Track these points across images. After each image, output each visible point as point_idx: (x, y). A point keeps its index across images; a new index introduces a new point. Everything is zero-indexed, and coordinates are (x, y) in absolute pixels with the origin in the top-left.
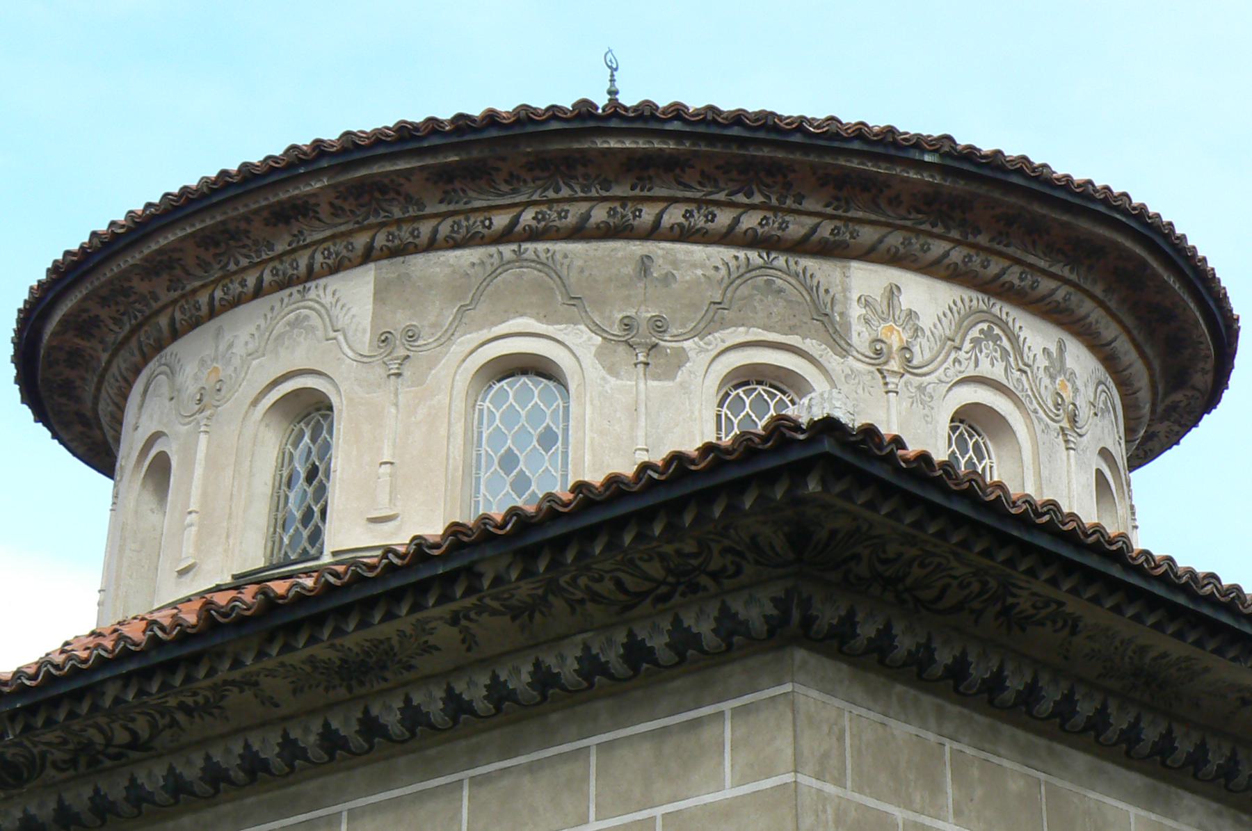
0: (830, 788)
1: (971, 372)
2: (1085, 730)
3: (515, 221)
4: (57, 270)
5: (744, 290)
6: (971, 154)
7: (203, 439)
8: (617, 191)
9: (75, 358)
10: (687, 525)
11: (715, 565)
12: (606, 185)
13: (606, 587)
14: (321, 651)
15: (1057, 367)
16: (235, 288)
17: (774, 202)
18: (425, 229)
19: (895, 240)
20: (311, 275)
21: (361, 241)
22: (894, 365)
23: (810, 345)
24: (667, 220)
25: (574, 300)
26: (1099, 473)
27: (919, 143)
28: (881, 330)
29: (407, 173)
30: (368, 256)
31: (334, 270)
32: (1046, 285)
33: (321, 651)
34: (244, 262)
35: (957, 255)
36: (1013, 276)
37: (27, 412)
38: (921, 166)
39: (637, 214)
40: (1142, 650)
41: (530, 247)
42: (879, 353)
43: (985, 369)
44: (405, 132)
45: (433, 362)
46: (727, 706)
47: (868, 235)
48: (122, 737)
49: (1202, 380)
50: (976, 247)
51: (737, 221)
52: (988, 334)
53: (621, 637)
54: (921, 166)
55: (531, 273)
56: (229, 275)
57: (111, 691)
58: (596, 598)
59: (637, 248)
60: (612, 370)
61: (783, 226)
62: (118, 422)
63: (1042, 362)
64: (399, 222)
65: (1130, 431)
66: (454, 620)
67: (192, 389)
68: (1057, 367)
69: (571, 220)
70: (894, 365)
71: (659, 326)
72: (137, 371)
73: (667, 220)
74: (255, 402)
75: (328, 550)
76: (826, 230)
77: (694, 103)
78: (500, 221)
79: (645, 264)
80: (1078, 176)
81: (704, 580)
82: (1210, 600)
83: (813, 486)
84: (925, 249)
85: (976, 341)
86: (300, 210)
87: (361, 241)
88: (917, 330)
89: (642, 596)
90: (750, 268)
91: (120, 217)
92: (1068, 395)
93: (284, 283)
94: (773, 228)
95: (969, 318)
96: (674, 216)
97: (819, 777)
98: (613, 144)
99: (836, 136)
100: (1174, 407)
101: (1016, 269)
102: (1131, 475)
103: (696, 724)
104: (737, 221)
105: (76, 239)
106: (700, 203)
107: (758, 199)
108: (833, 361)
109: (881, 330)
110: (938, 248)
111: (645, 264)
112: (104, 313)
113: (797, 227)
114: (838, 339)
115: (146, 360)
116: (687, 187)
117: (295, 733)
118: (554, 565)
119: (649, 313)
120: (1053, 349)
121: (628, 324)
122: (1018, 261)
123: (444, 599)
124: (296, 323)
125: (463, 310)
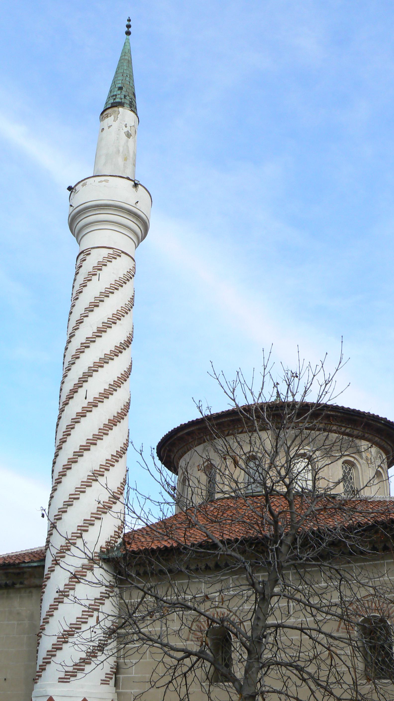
17: (353, 427)
23: (357, 457)
24: (333, 429)
27: (382, 419)
34: (239, 426)
42: (367, 459)
50: (381, 439)
51: (345, 430)
61: (353, 432)
70: (369, 462)
77: (346, 406)
94: (351, 433)
104: (345, 430)
106: (339, 426)
107: (350, 426)
113: (356, 432)
116: (338, 422)
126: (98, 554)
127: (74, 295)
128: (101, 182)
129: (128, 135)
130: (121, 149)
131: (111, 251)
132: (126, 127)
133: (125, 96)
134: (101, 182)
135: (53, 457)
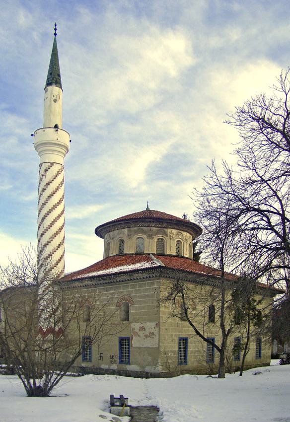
10: (6, 365)
47: (169, 227)
71: (152, 235)
79: (150, 230)
96: (153, 225)
102: (272, 360)
111: (150, 230)
114: (167, 236)
131: (49, 164)
132: (54, 96)
133: (53, 78)
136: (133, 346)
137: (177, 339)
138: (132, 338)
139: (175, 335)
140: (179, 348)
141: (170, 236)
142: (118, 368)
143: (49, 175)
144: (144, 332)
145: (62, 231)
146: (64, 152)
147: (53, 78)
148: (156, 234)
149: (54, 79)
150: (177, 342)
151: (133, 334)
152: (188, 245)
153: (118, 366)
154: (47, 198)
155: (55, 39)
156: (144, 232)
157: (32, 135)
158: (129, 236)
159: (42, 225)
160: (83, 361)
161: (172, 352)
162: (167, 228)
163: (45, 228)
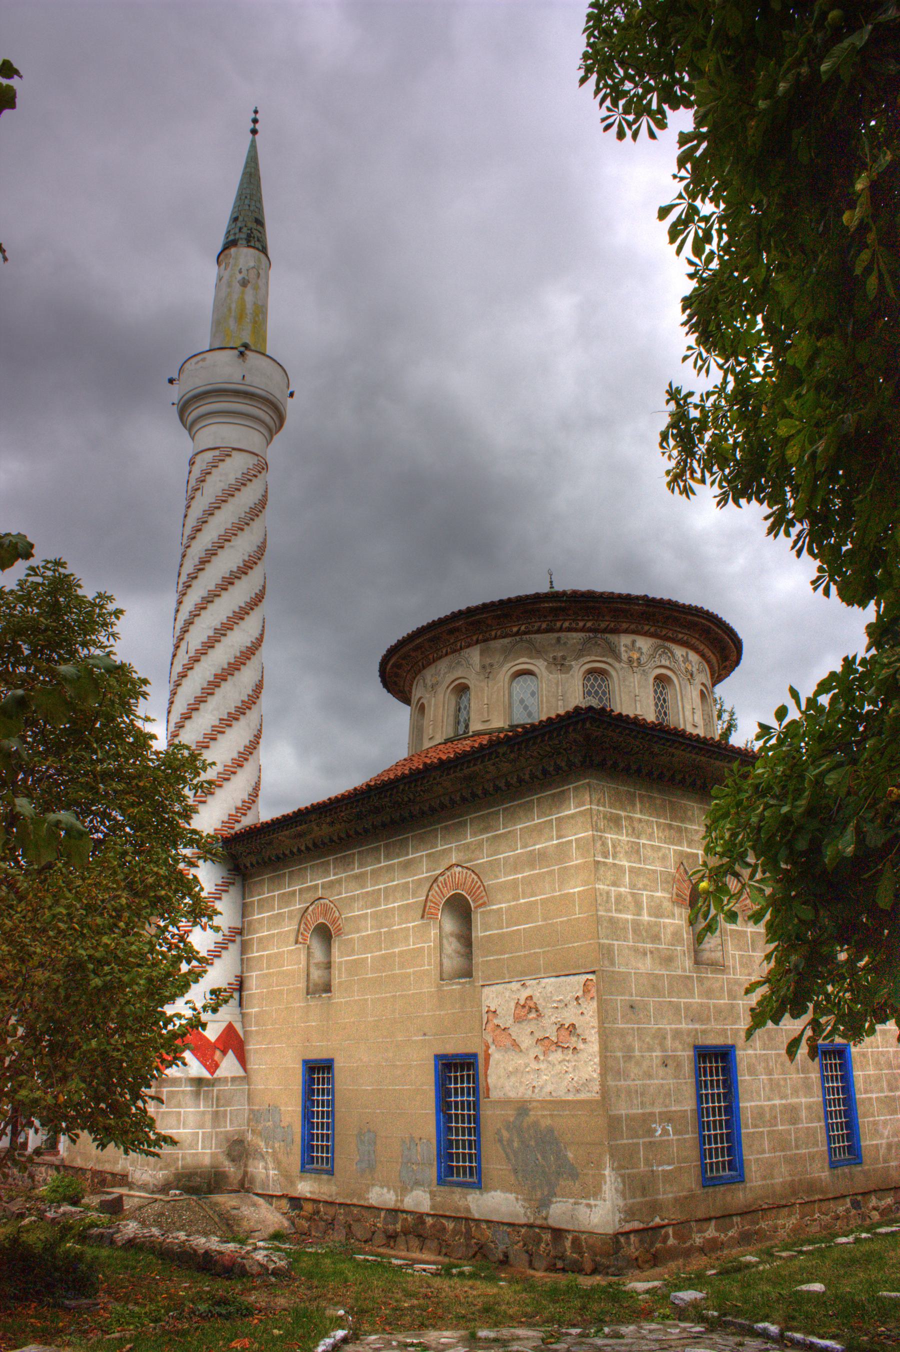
0: (601, 808)
1: (659, 664)
2: (679, 784)
3: (519, 629)
4: (388, 651)
5: (589, 645)
6: (654, 600)
7: (433, 699)
8: (549, 618)
9: (397, 675)
11: (565, 747)
12: (545, 617)
13: (535, 754)
14: (458, 774)
15: (686, 659)
16: (440, 653)
18: (493, 633)
19: (633, 627)
20: (461, 648)
21: (475, 638)
22: (635, 664)
23: (609, 660)
24: (564, 626)
25: (538, 652)
26: (702, 691)
28: (631, 654)
29: (486, 618)
30: (477, 642)
31: (468, 646)
32: (680, 636)
33: (458, 774)
35: (652, 630)
36: (670, 634)
37: (385, 690)
38: (639, 605)
39: (555, 625)
40: (694, 760)
41: (524, 637)
43: (663, 663)
44: (485, 606)
45: (499, 673)
46: (571, 786)
47: (625, 626)
48: (406, 799)
49: (733, 658)
50: (659, 627)
51: (585, 625)
52: (664, 652)
53: (540, 767)
54: (639, 605)
55: (525, 645)
56: (438, 650)
57: (401, 787)
58: (532, 756)
59: (556, 635)
60: (551, 672)
61: (599, 625)
62: (411, 692)
63: (681, 659)
64: (486, 632)
65: (712, 675)
66: (494, 765)
67: (429, 684)
68: (686, 659)
69: (536, 628)
70: (635, 664)
71: (564, 658)
72: (414, 678)
73: (564, 626)
74: (448, 687)
75: (471, 730)
76: (612, 625)
78: (515, 629)
80: (687, 603)
81: (562, 751)
82: (712, 745)
83: (588, 725)
84: (642, 628)
85: (660, 655)
86: (457, 630)
87: (475, 638)
88: (642, 653)
89: (546, 756)
90: (590, 638)
91: (405, 635)
92: (689, 668)
93: (455, 651)
95: (656, 648)
96: (566, 624)
97: (598, 805)
98: (546, 605)
99: (613, 598)
100: (725, 667)
101: (671, 632)
103: (563, 791)
105: (393, 642)
108: (617, 665)
109: (631, 654)
110: (646, 628)
111: (558, 640)
112: (403, 662)
113: (603, 625)
114: (618, 658)
115: (416, 675)
117: (453, 797)
118: (519, 749)
119: (560, 654)
120: (684, 654)
121: (555, 658)
122: (671, 630)
123: (489, 759)
124: (459, 663)
125: (506, 657)
126: (858, 271)
127: (189, 493)
128: (197, 363)
129: (244, 283)
130: (233, 306)
131: (217, 453)
132: (240, 272)
133: (240, 229)
134: (197, 363)
135: (167, 706)
136: (495, 1095)
137: (686, 1055)
138: (488, 1057)
139: (677, 1034)
140: (700, 1098)
141: (630, 661)
142: (433, 1207)
143: (214, 487)
144: (532, 1027)
145: (253, 663)
146: (272, 424)
147: (240, 229)
148: (580, 654)
149: (245, 230)
150: (688, 1068)
151: (490, 1041)
152: (696, 695)
153: (433, 1195)
154: (203, 555)
155: (253, 146)
156: (537, 652)
157: (171, 381)
158: (487, 671)
159: (183, 645)
160: (303, 1170)
161: (670, 1120)
162: (615, 631)
163: (192, 653)
